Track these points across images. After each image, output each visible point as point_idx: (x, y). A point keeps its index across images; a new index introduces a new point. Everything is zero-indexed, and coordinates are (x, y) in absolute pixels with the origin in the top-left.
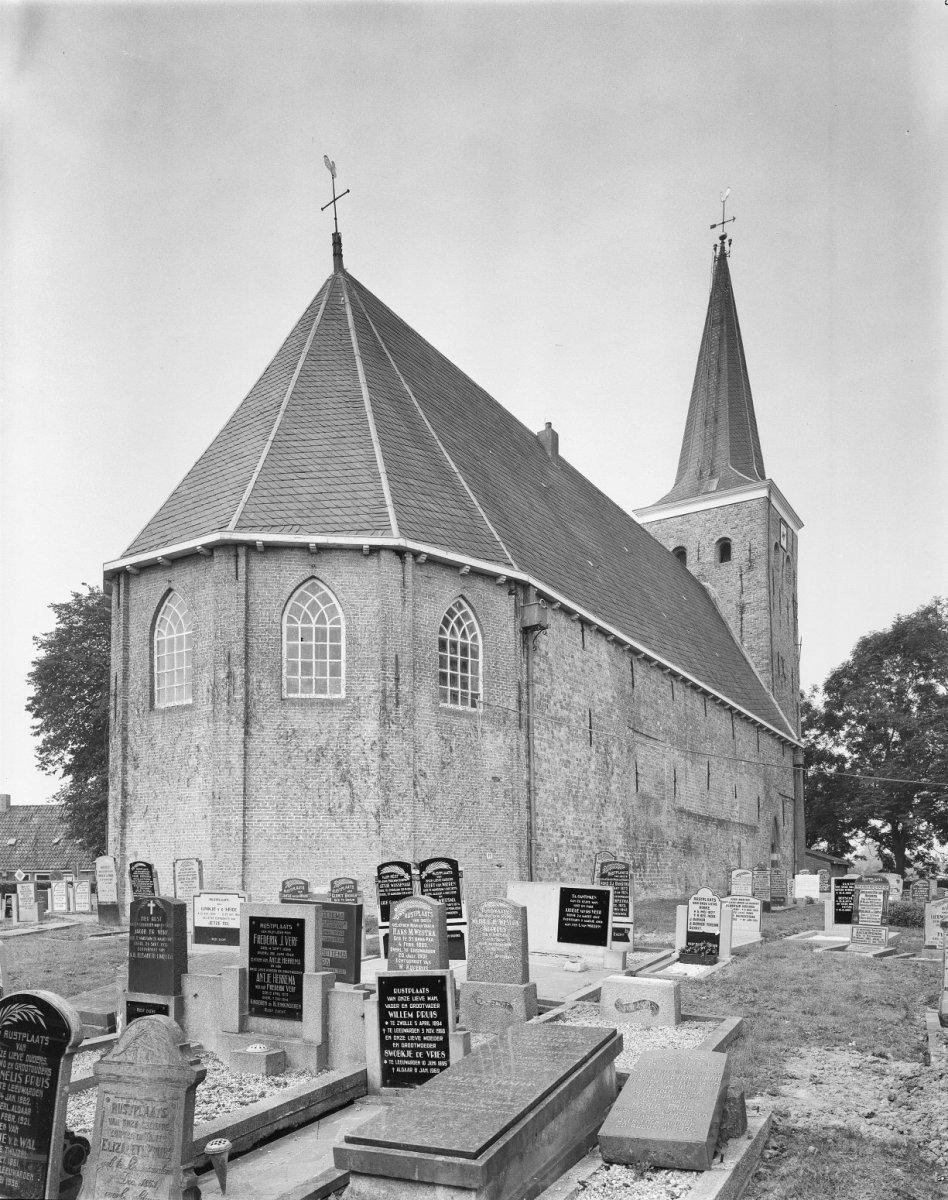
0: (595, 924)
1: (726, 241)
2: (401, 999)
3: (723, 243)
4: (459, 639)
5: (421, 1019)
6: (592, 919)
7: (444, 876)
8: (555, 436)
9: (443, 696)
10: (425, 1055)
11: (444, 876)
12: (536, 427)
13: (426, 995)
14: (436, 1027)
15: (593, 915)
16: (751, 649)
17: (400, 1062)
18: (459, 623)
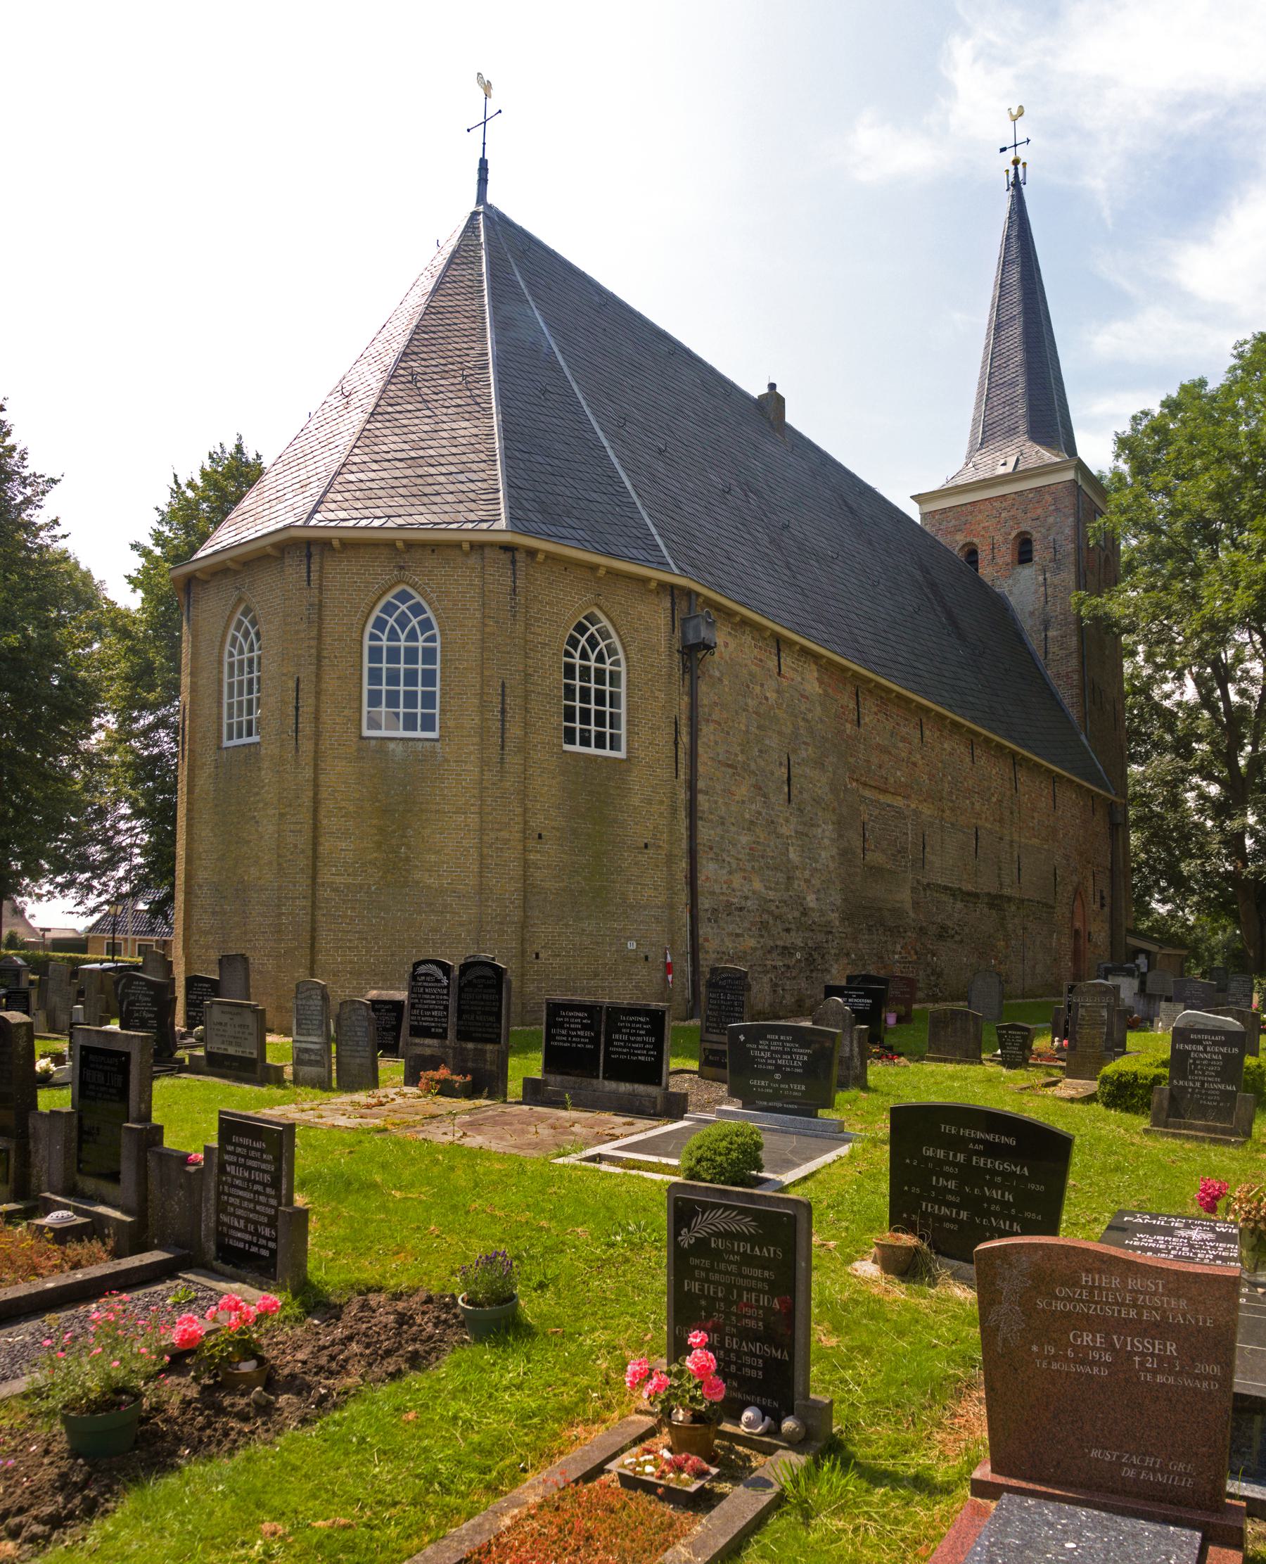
0: (647, 1055)
1: (1020, 166)
2: (239, 1150)
3: (1016, 169)
4: (593, 664)
5: (255, 1182)
6: (644, 1049)
7: (486, 986)
8: (780, 401)
9: (569, 736)
10: (256, 1229)
11: (486, 986)
12: (756, 389)
13: (262, 1151)
14: (268, 1196)
15: (645, 1043)
16: (1058, 675)
17: (233, 1232)
18: (592, 642)
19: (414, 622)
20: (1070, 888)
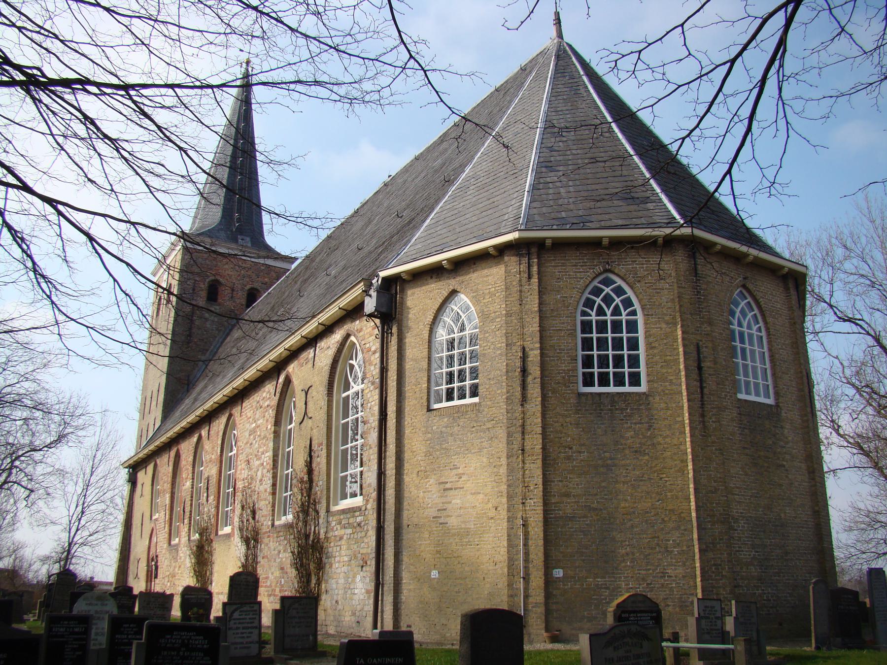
9: (588, 381)
19: (598, 301)
20: (249, 511)
